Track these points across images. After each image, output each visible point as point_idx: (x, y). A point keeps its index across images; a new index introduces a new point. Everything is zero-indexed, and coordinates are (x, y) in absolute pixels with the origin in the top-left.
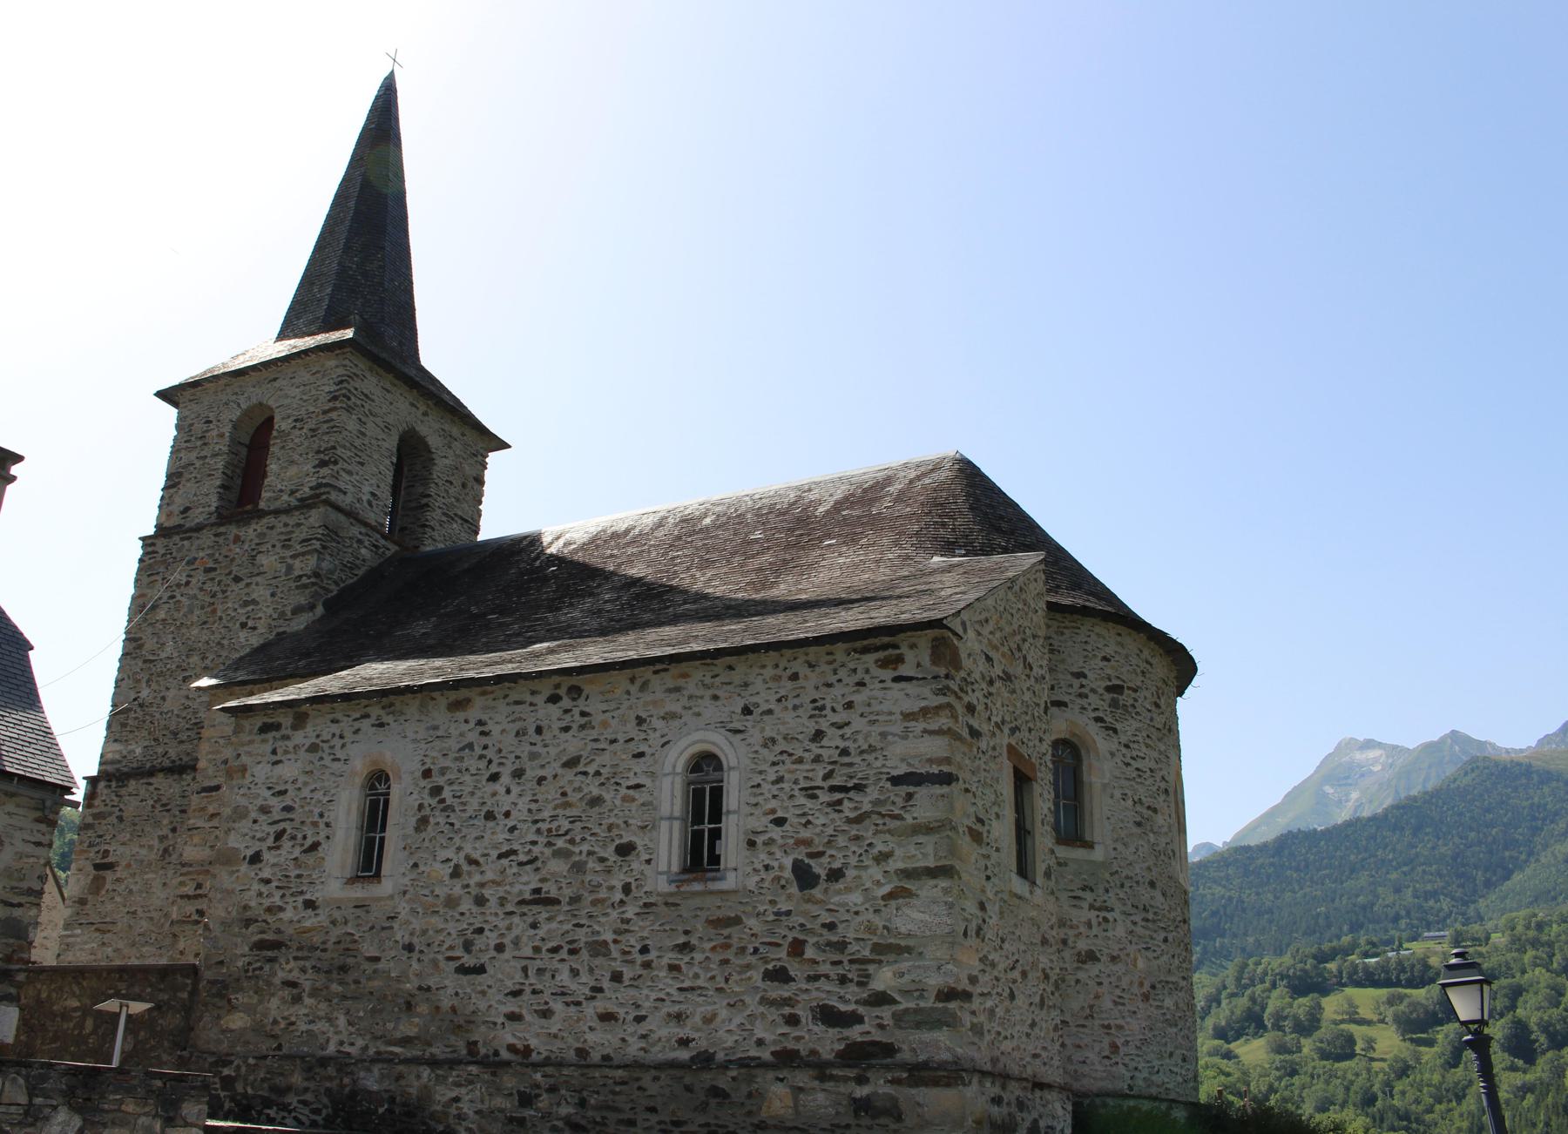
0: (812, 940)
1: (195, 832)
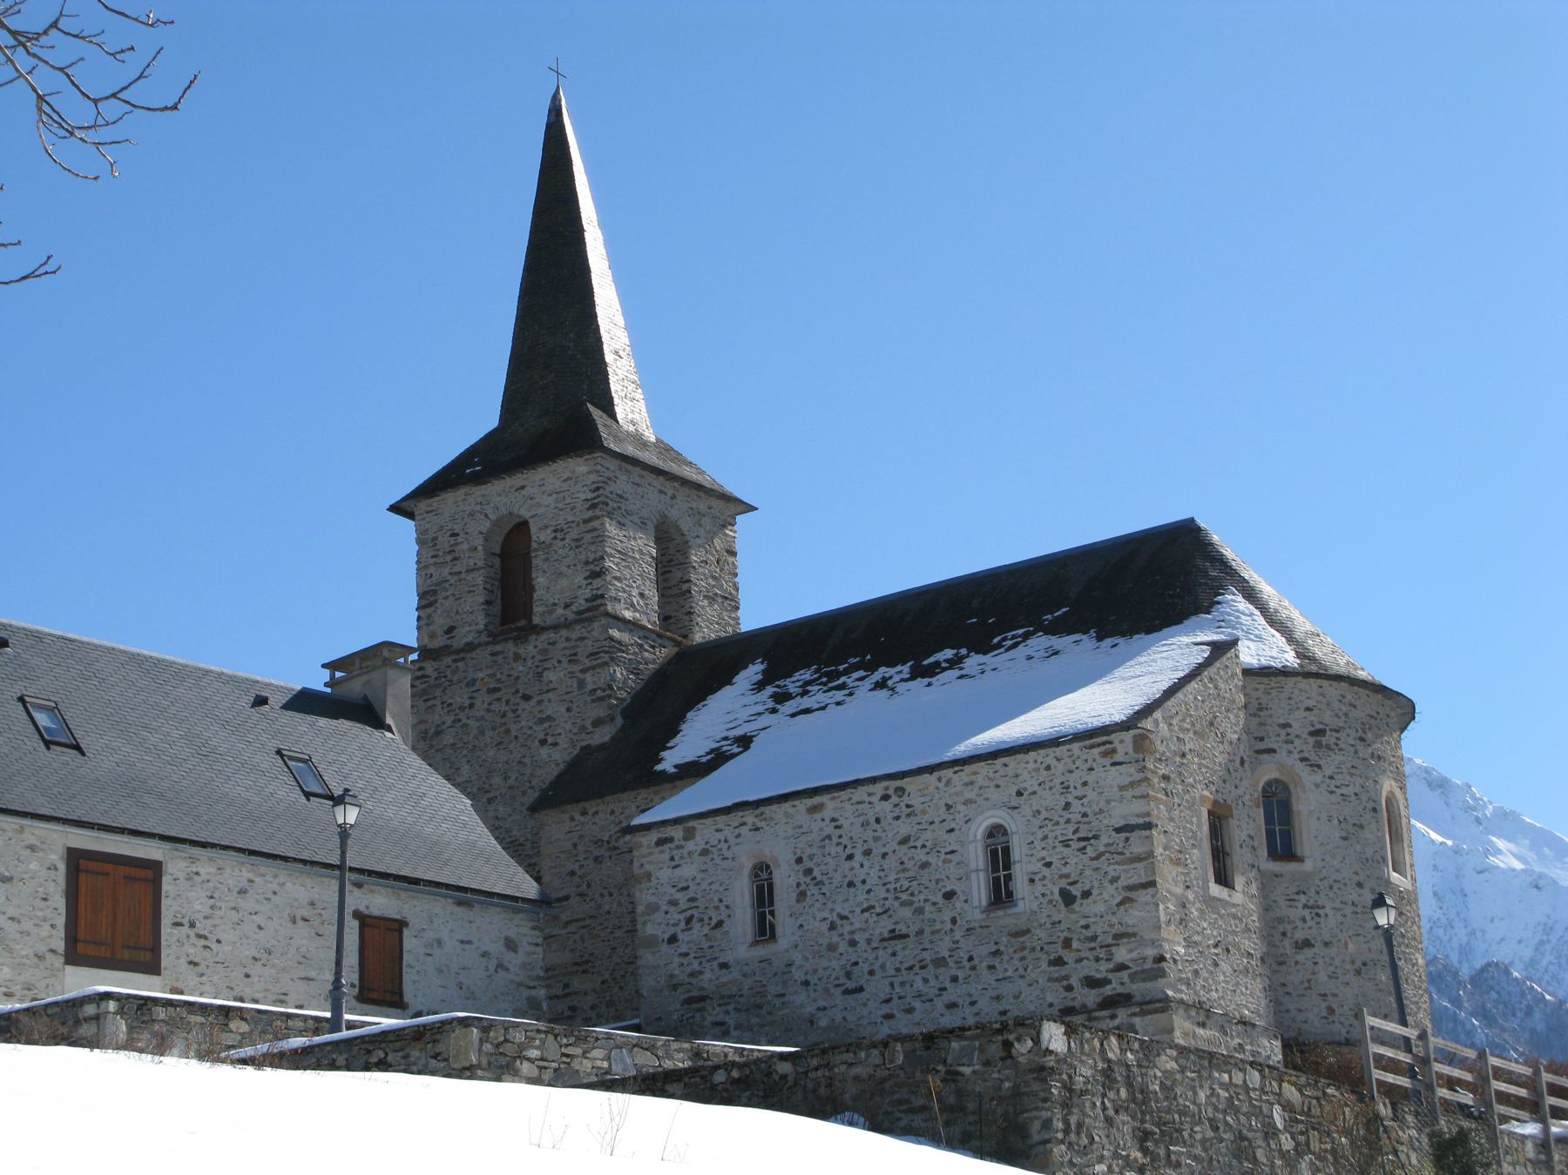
0: (1075, 937)
1: (552, 939)
